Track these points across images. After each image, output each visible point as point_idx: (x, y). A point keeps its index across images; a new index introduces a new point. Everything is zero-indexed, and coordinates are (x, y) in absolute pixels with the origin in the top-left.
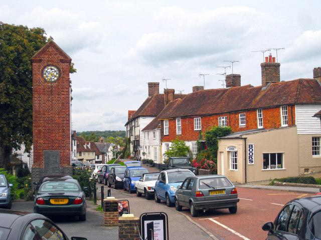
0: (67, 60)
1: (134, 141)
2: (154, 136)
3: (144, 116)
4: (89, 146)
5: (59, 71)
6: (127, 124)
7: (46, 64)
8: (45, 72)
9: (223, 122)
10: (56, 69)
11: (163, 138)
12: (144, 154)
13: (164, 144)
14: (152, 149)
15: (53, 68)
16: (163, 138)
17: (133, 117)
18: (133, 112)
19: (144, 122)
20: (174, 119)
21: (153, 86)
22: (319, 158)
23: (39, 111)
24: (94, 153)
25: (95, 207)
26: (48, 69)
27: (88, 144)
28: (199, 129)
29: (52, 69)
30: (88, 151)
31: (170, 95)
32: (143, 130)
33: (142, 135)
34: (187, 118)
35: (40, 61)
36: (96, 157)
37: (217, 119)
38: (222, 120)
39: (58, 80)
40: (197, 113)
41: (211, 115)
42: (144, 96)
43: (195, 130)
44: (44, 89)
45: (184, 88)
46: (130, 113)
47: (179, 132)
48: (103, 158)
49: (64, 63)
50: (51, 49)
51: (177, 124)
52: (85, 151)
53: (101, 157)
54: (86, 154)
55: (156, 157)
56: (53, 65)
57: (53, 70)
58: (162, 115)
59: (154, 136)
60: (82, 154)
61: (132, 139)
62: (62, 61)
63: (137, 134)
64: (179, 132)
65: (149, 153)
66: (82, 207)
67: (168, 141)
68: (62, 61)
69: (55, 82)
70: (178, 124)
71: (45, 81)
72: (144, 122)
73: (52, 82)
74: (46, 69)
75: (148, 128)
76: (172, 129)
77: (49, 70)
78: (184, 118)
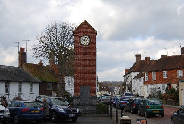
0: (94, 33)
1: (129, 84)
2: (140, 82)
3: (134, 71)
4: (105, 87)
5: (90, 39)
6: (124, 76)
7: (82, 35)
8: (81, 40)
9: (180, 73)
10: (88, 38)
11: (145, 83)
12: (134, 91)
13: (145, 85)
14: (139, 89)
15: (86, 37)
16: (145, 83)
17: (128, 72)
18: (127, 70)
19: (134, 74)
20: (152, 72)
21: (138, 56)
22: (124, 116)
23: (78, 63)
24: (107, 91)
25: (147, 93)
26: (83, 38)
27: (104, 86)
28: (166, 77)
29: (86, 38)
30: (104, 90)
31: (148, 60)
32: (134, 78)
33: (133, 81)
34: (159, 71)
35: (79, 33)
36: (108, 93)
37: (177, 71)
38: (180, 72)
39: (89, 44)
40: (165, 69)
41: (173, 69)
42: (134, 60)
43: (163, 78)
44: (81, 50)
45: (156, 56)
46: (126, 70)
47: (154, 79)
48: (112, 94)
49: (93, 34)
50: (85, 26)
51: (153, 74)
52: (103, 90)
53: (110, 93)
54: (103, 91)
55: (141, 93)
56: (86, 35)
57: (86, 39)
58: (144, 70)
59: (140, 82)
60: (101, 91)
61: (127, 83)
62: (91, 33)
63: (130, 81)
64: (154, 79)
65: (137, 91)
66: (137, 113)
67: (148, 84)
68: (91, 33)
69: (87, 45)
70: (154, 75)
71: (82, 45)
72: (134, 74)
73: (85, 46)
74: (82, 38)
75: (137, 77)
76: (150, 78)
77: (84, 38)
78: (157, 71)
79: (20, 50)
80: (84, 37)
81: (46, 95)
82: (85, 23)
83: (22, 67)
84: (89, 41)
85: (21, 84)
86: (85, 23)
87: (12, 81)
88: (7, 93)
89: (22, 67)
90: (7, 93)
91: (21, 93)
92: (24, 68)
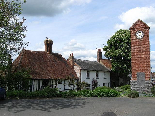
5: (144, 33)
7: (137, 30)
29: (140, 33)
44: (136, 42)
49: (146, 29)
50: (139, 23)
56: (140, 31)
60: (153, 78)
68: (145, 28)
69: (142, 38)
74: (137, 33)
77: (139, 33)
79: (98, 51)
80: (139, 32)
81: (10, 102)
82: (139, 21)
83: (99, 61)
84: (143, 35)
85: (97, 72)
86: (139, 21)
87: (91, 70)
88: (88, 78)
89: (99, 61)
90: (88, 78)
91: (105, 78)
92: (101, 62)
